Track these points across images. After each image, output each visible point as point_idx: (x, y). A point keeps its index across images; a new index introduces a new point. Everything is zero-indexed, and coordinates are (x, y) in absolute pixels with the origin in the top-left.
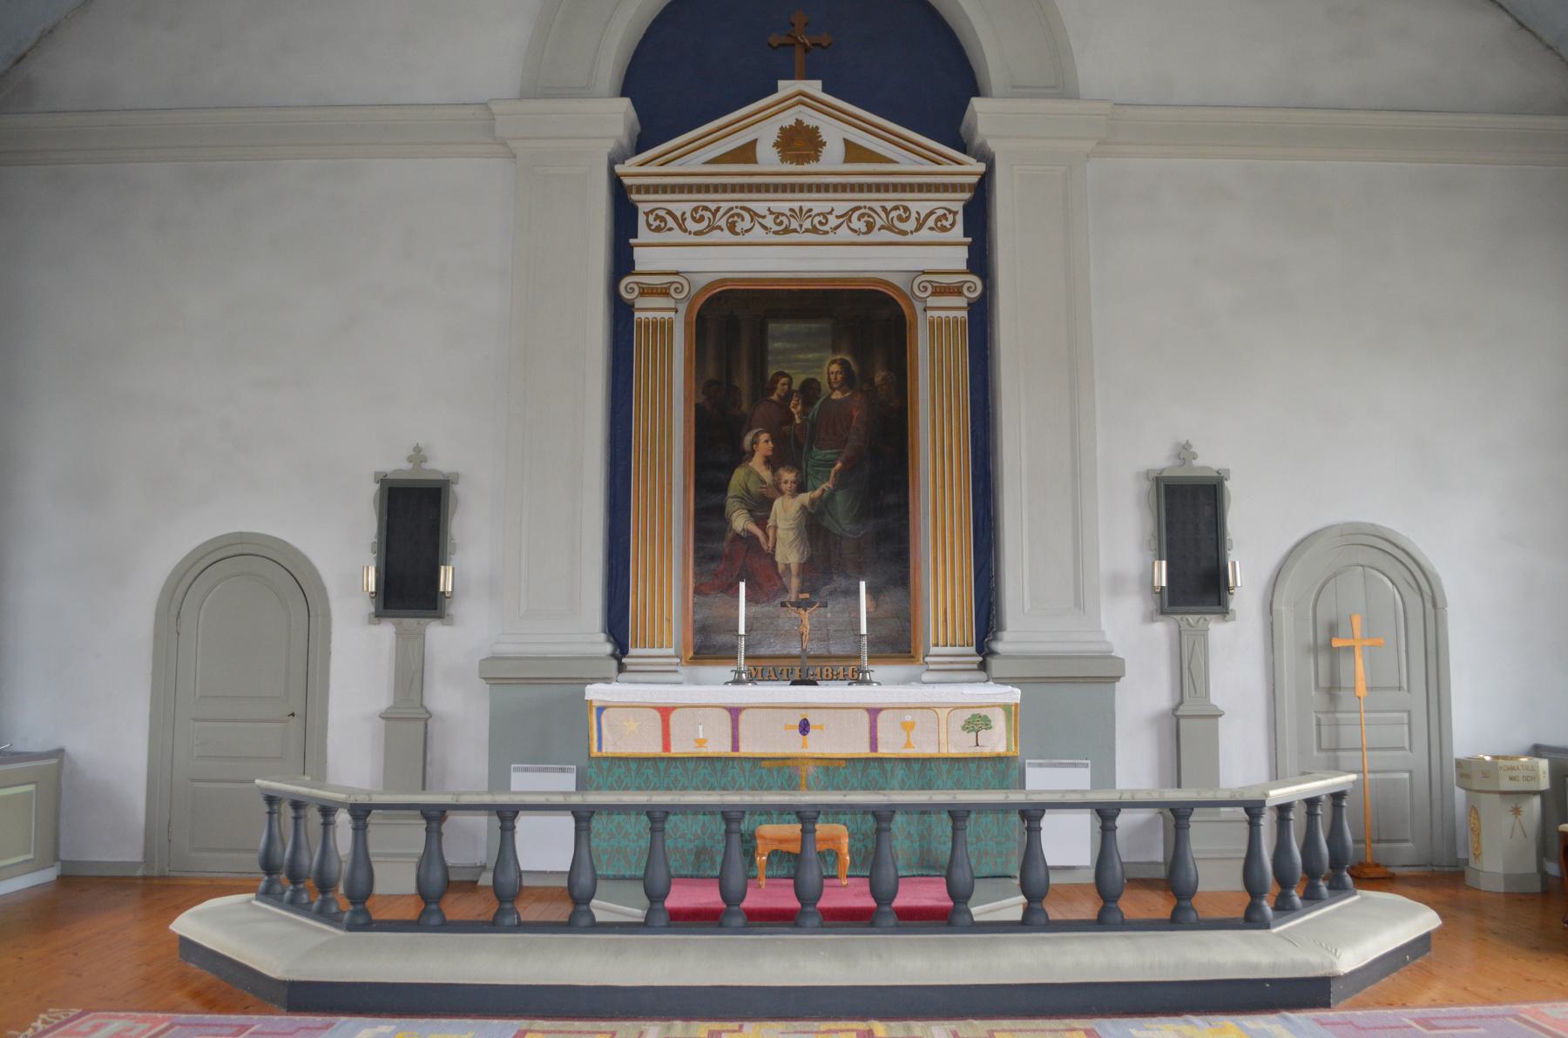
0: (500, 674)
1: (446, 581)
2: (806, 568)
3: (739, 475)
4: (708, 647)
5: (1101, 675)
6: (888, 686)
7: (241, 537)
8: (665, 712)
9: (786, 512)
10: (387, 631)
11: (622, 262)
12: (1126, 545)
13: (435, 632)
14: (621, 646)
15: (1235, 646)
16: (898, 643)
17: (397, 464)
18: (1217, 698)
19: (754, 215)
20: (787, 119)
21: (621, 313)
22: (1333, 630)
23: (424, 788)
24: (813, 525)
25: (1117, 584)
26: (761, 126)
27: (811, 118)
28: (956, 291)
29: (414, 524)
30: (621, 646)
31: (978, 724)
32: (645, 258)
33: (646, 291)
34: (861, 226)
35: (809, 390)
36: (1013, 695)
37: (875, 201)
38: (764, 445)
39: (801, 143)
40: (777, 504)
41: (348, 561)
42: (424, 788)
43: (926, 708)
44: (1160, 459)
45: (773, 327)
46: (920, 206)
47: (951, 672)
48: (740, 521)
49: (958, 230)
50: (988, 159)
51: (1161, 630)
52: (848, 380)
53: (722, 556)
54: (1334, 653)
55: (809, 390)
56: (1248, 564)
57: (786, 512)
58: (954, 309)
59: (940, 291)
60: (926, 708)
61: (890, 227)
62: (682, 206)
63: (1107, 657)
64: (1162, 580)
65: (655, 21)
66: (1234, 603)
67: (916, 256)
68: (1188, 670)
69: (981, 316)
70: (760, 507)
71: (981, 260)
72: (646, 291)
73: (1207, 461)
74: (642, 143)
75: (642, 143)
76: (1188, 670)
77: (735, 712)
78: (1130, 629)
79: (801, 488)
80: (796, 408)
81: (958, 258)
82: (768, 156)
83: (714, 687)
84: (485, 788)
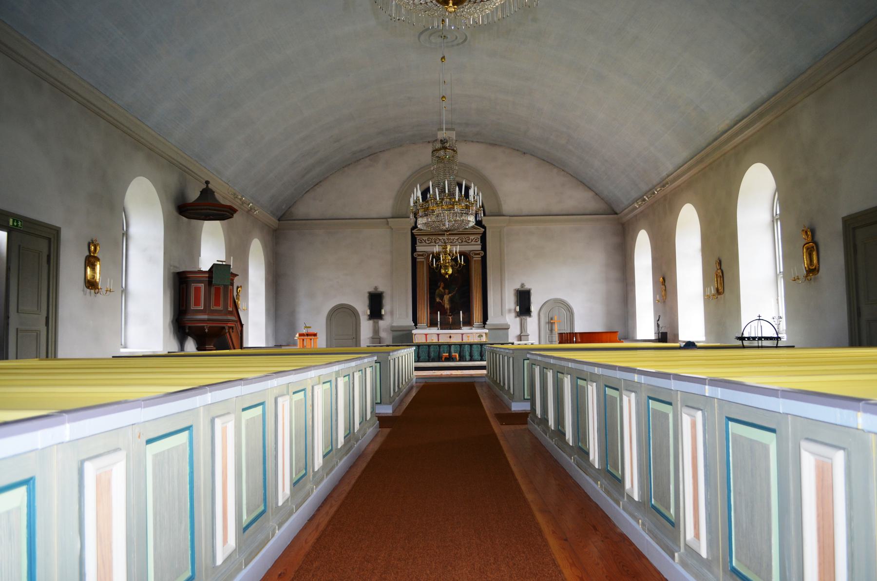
0: (393, 330)
1: (383, 312)
2: (450, 308)
3: (437, 291)
4: (433, 324)
5: (506, 328)
6: (465, 330)
7: (350, 306)
8: (426, 335)
9: (446, 298)
10: (371, 322)
11: (414, 250)
12: (510, 302)
13: (381, 323)
14: (416, 325)
15: (532, 323)
16: (469, 323)
17: (371, 290)
18: (529, 332)
21: (414, 260)
22: (552, 319)
23: (47, 357)
24: (451, 300)
25: (510, 311)
28: (479, 254)
29: (376, 302)
30: (416, 325)
31: (480, 336)
32: (419, 249)
33: (419, 255)
36: (487, 331)
37: (463, 236)
38: (442, 285)
41: (362, 308)
42: (47, 357)
43: (471, 334)
44: (518, 287)
46: (472, 237)
47: (478, 328)
48: (438, 300)
50: (484, 227)
51: (518, 319)
53: (435, 307)
54: (552, 324)
56: (534, 308)
57: (446, 298)
58: (478, 258)
59: (476, 254)
60: (471, 334)
62: (425, 238)
63: (507, 324)
64: (518, 309)
66: (532, 314)
68: (523, 327)
69: (484, 260)
70: (442, 297)
71: (484, 248)
72: (419, 255)
73: (527, 287)
76: (523, 327)
77: (438, 335)
78: (512, 321)
79: (449, 293)
81: (479, 247)
83: (434, 330)
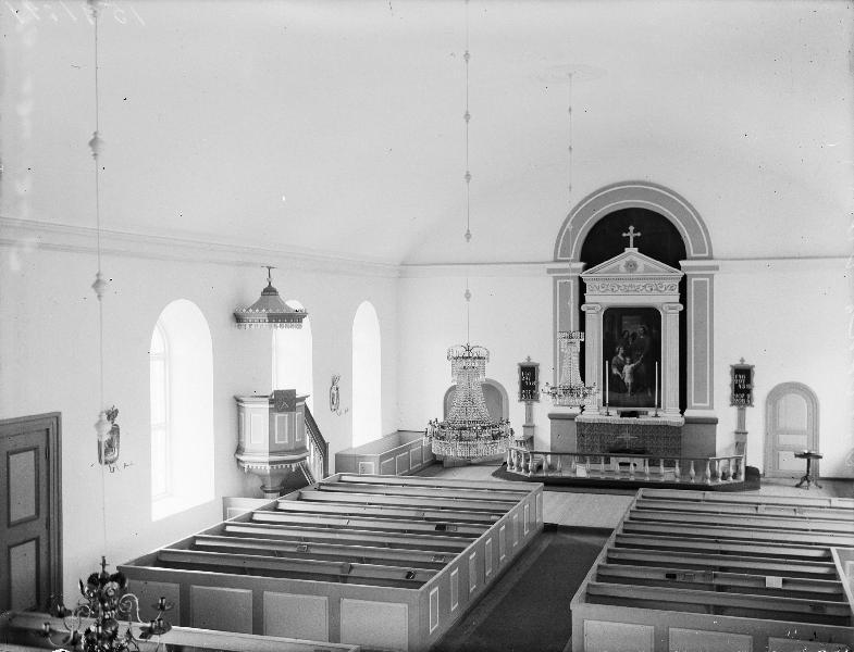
3: (615, 359)
12: (723, 384)
15: (755, 415)
18: (747, 429)
19: (619, 287)
20: (627, 259)
26: (618, 262)
27: (635, 259)
29: (529, 373)
34: (648, 289)
35: (634, 335)
38: (621, 351)
39: (631, 266)
40: (626, 367)
41: (512, 387)
45: (624, 318)
46: (666, 283)
49: (677, 290)
52: (645, 333)
55: (634, 335)
57: (627, 369)
61: (657, 289)
65: (606, 217)
67: (665, 300)
69: (683, 316)
70: (621, 369)
71: (683, 300)
74: (586, 268)
75: (586, 268)
76: (741, 421)
79: (632, 362)
80: (630, 340)
81: (677, 298)
82: (622, 269)
84: (551, 257)
